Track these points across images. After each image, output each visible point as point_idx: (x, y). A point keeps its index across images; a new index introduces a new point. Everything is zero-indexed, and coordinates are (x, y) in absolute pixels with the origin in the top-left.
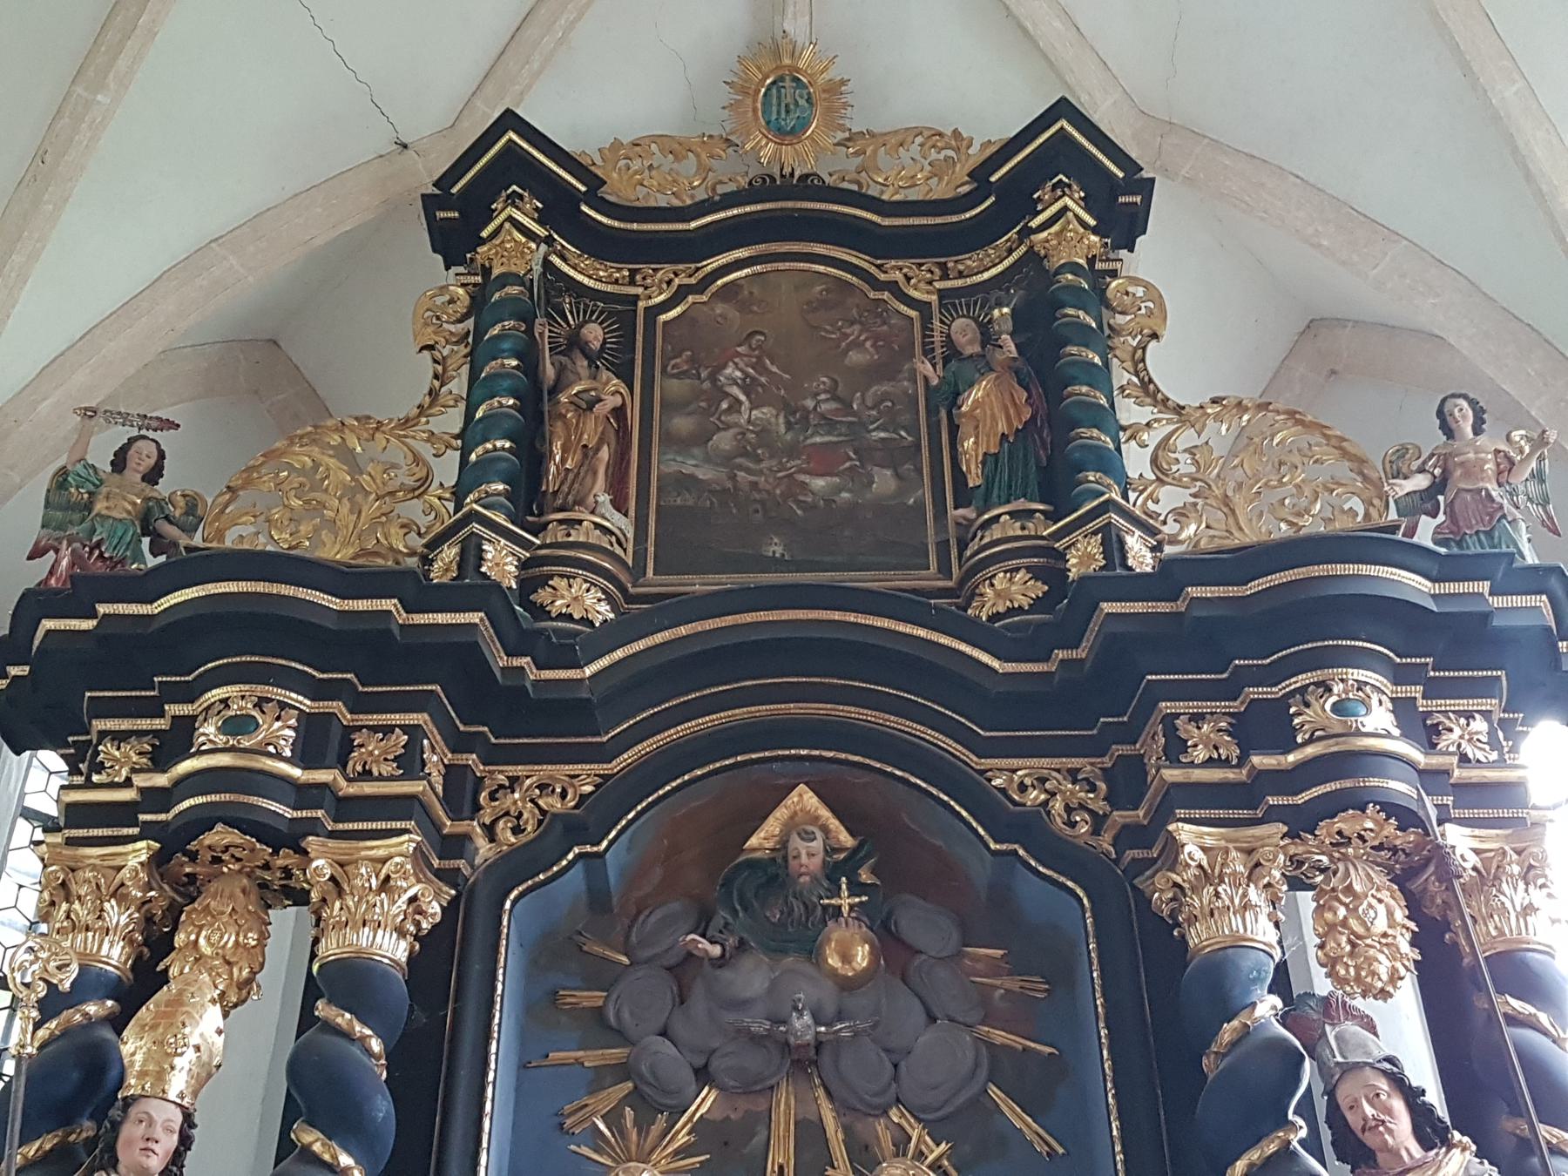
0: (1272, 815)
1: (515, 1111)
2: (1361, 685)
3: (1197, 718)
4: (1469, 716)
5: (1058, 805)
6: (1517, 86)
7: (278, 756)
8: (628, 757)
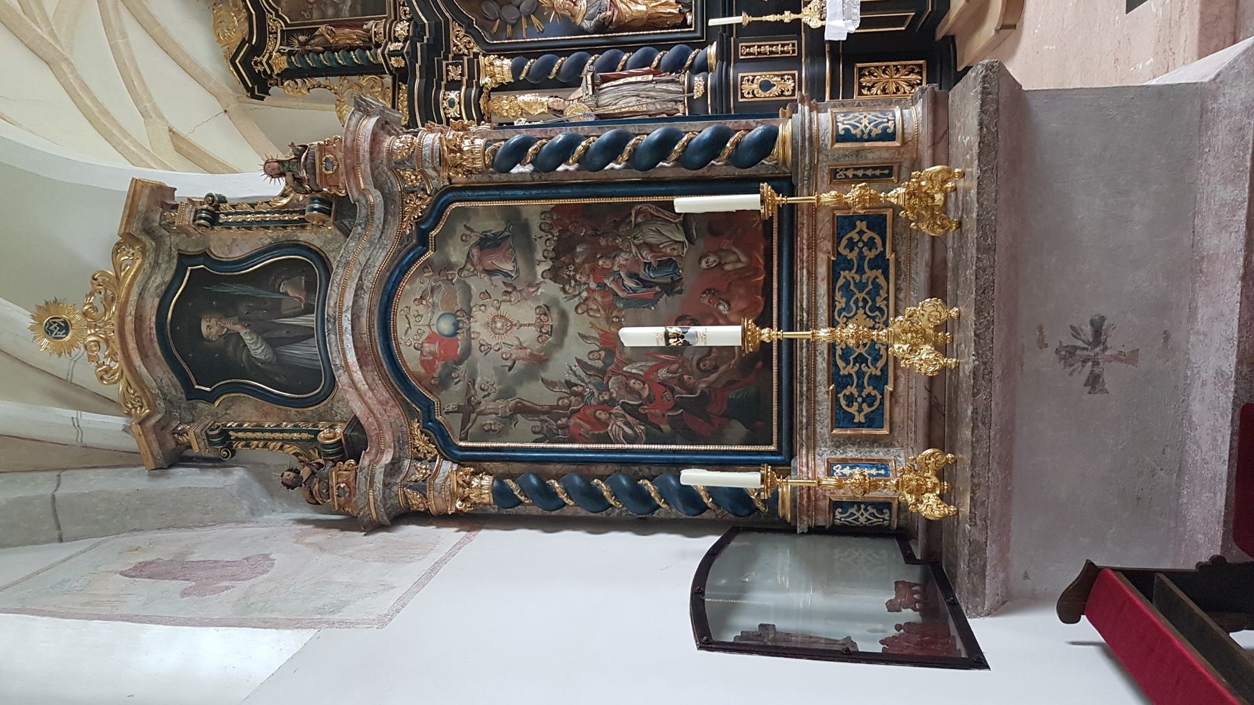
7: (460, 94)
8: (447, 14)
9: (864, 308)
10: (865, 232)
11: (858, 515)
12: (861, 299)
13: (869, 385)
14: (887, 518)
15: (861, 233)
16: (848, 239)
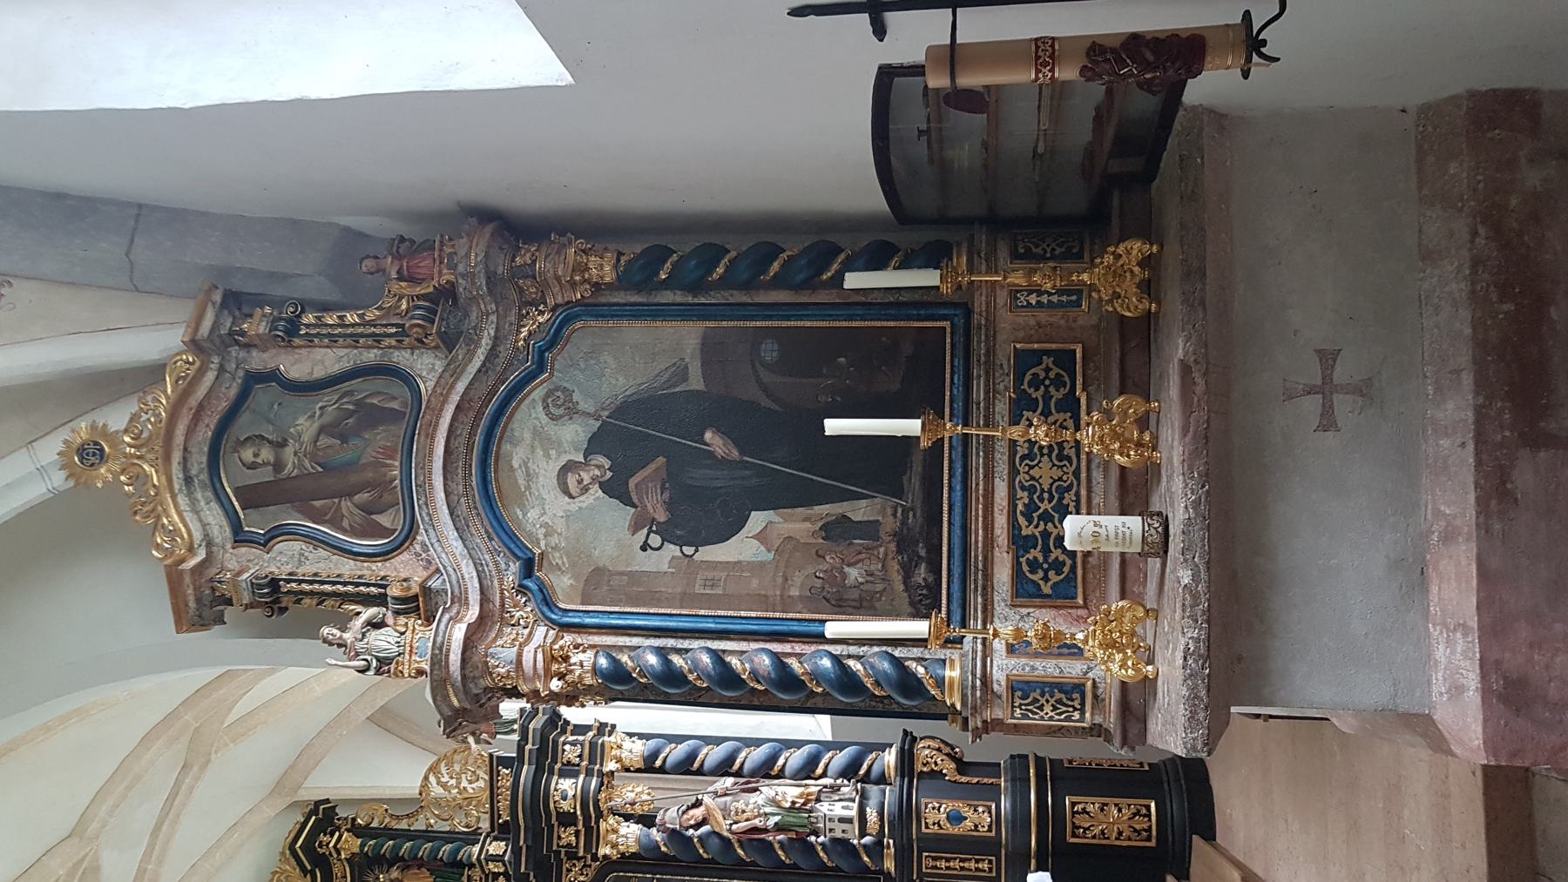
0: (597, 823)
1: (889, 101)
2: (556, 790)
3: (559, 838)
4: (564, 751)
6: (316, 686)
7: (576, 783)
9: (1050, 456)
10: (1051, 369)
11: (1043, 701)
12: (1046, 502)
13: (1056, 548)
14: (1079, 707)
15: (1048, 370)
16: (1033, 374)
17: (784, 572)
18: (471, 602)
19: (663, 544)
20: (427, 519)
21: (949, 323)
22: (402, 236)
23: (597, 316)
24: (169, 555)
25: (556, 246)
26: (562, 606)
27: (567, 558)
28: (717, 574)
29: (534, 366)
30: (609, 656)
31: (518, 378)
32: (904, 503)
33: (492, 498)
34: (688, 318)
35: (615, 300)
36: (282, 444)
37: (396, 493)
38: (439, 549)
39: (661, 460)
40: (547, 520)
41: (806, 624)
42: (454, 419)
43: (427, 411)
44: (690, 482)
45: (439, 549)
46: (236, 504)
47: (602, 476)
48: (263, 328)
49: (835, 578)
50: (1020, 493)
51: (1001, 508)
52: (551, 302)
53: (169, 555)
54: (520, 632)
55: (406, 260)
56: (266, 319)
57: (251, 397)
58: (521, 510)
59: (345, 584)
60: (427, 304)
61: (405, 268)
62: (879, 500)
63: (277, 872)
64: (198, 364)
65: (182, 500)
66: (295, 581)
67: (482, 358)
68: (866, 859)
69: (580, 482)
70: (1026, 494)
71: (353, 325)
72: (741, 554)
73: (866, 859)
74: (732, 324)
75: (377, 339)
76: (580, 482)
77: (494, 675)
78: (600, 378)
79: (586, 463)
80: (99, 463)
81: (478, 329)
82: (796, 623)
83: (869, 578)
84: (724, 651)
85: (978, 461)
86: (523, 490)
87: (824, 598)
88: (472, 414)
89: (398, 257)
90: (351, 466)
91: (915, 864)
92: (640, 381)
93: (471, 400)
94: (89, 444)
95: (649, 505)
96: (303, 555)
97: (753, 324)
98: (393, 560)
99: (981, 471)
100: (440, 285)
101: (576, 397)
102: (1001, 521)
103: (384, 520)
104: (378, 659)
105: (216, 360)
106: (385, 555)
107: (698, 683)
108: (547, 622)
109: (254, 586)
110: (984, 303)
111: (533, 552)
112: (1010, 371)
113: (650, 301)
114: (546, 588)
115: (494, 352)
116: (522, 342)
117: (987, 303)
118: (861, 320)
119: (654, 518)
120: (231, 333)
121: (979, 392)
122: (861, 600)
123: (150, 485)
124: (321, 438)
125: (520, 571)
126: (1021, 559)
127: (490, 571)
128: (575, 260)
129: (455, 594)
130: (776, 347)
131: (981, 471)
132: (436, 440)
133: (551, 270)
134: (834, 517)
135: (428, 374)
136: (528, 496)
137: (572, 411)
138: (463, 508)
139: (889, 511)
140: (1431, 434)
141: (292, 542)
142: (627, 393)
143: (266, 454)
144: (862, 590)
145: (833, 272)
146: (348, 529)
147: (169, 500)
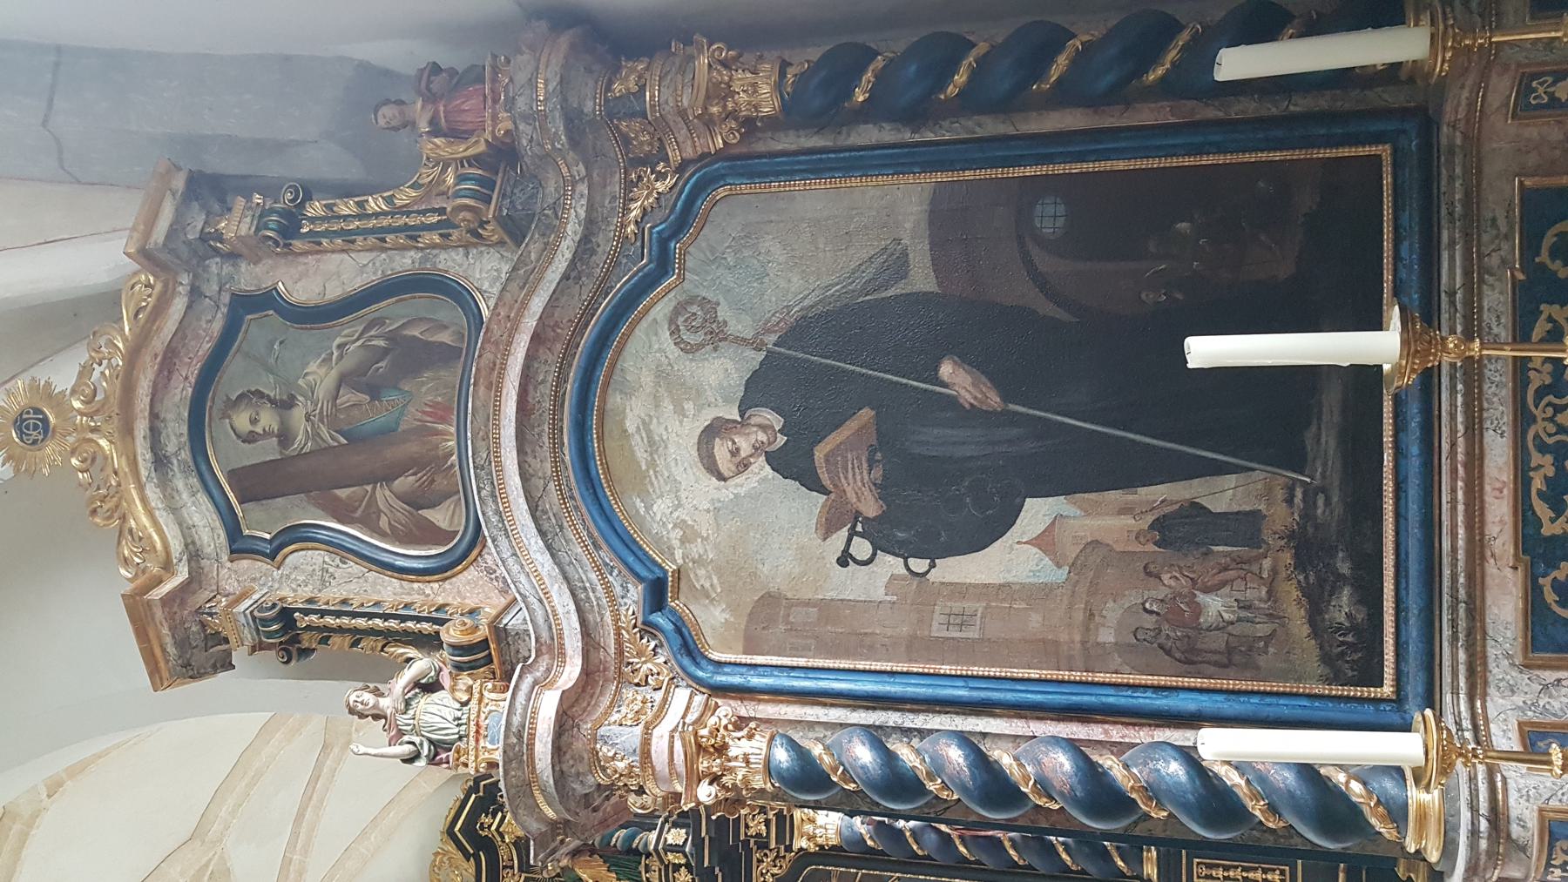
3: (747, 826)
5: (775, 871)
17: (1087, 602)
18: (569, 652)
19: (874, 554)
20: (494, 519)
21: (1387, 147)
22: (434, 63)
23: (753, 175)
24: (140, 572)
25: (678, 61)
26: (715, 656)
27: (719, 578)
28: (969, 605)
29: (652, 266)
30: (793, 745)
31: (627, 286)
32: (1308, 480)
33: (596, 482)
34: (906, 170)
35: (780, 147)
36: (285, 405)
37: (454, 475)
38: (515, 568)
39: (866, 414)
40: (683, 517)
41: (1129, 693)
42: (530, 358)
43: (487, 346)
44: (917, 450)
45: (515, 568)
46: (231, 495)
47: (770, 444)
48: (246, 228)
49: (1181, 613)
50: (1536, 458)
51: (1498, 485)
52: (675, 156)
53: (140, 572)
54: (648, 697)
55: (443, 102)
56: (250, 213)
57: (241, 335)
58: (642, 501)
59: (386, 617)
60: (480, 172)
61: (442, 115)
62: (1260, 475)
63: (439, 853)
64: (159, 287)
65: (153, 493)
66: (315, 612)
67: (569, 255)
68: (1120, 863)
69: (735, 453)
70: (1549, 458)
71: (376, 215)
72: (1009, 572)
73: (1120, 863)
74: (981, 174)
75: (413, 233)
76: (735, 453)
77: (609, 771)
78: (760, 279)
79: (743, 423)
80: (43, 440)
81: (558, 208)
82: (1111, 691)
83: (1243, 614)
84: (984, 735)
85: (1451, 402)
86: (644, 468)
87: (1161, 647)
88: (559, 347)
89: (431, 98)
90: (387, 433)
91: (1184, 872)
92: (826, 281)
93: (556, 325)
94: (28, 413)
95: (849, 490)
96: (327, 571)
97: (1018, 172)
98: (454, 579)
99: (1460, 419)
100: (494, 137)
101: (723, 313)
102: (1499, 512)
103: (439, 517)
104: (431, 741)
105: (185, 279)
106: (443, 569)
107: (944, 795)
108: (690, 683)
109: (259, 622)
110: (1464, 102)
111: (662, 568)
112: (1512, 228)
113: (839, 143)
114: (686, 627)
115: (589, 246)
116: (632, 227)
117: (1469, 105)
118: (1219, 152)
119: (857, 511)
120: (204, 238)
121: (1451, 271)
122: (1230, 650)
123: (109, 470)
124: (341, 392)
125: (644, 600)
126: (1541, 581)
127: (598, 599)
128: (710, 80)
129: (543, 640)
130: (1061, 209)
131: (1460, 419)
132: (504, 392)
133: (671, 99)
134: (1176, 507)
135: (491, 286)
136: (653, 477)
137: (717, 337)
138: (553, 498)
139: (1280, 494)
140: (155, 281)
141: (310, 552)
142: (806, 303)
143: (268, 419)
144: (1230, 634)
145: (1168, 66)
146: (388, 531)
147: (134, 493)
